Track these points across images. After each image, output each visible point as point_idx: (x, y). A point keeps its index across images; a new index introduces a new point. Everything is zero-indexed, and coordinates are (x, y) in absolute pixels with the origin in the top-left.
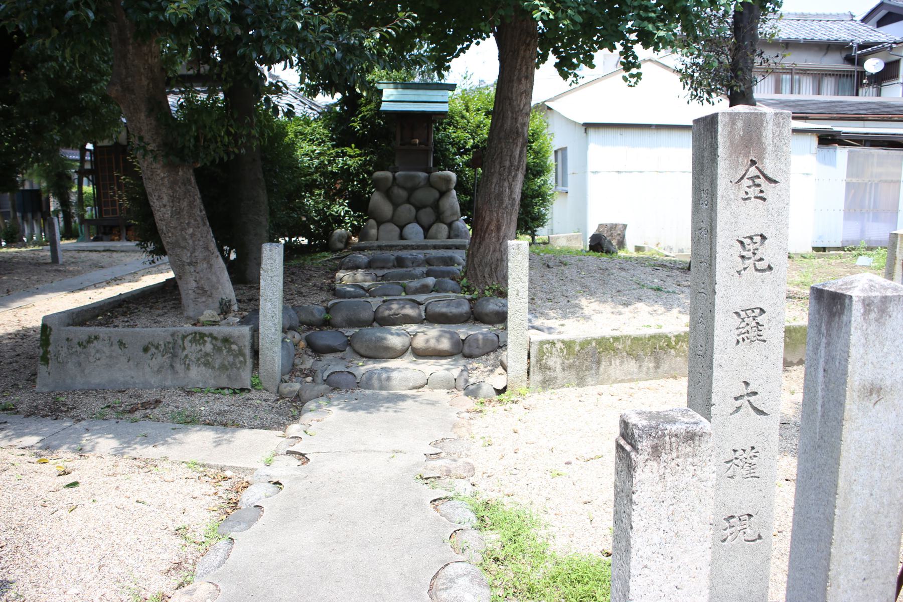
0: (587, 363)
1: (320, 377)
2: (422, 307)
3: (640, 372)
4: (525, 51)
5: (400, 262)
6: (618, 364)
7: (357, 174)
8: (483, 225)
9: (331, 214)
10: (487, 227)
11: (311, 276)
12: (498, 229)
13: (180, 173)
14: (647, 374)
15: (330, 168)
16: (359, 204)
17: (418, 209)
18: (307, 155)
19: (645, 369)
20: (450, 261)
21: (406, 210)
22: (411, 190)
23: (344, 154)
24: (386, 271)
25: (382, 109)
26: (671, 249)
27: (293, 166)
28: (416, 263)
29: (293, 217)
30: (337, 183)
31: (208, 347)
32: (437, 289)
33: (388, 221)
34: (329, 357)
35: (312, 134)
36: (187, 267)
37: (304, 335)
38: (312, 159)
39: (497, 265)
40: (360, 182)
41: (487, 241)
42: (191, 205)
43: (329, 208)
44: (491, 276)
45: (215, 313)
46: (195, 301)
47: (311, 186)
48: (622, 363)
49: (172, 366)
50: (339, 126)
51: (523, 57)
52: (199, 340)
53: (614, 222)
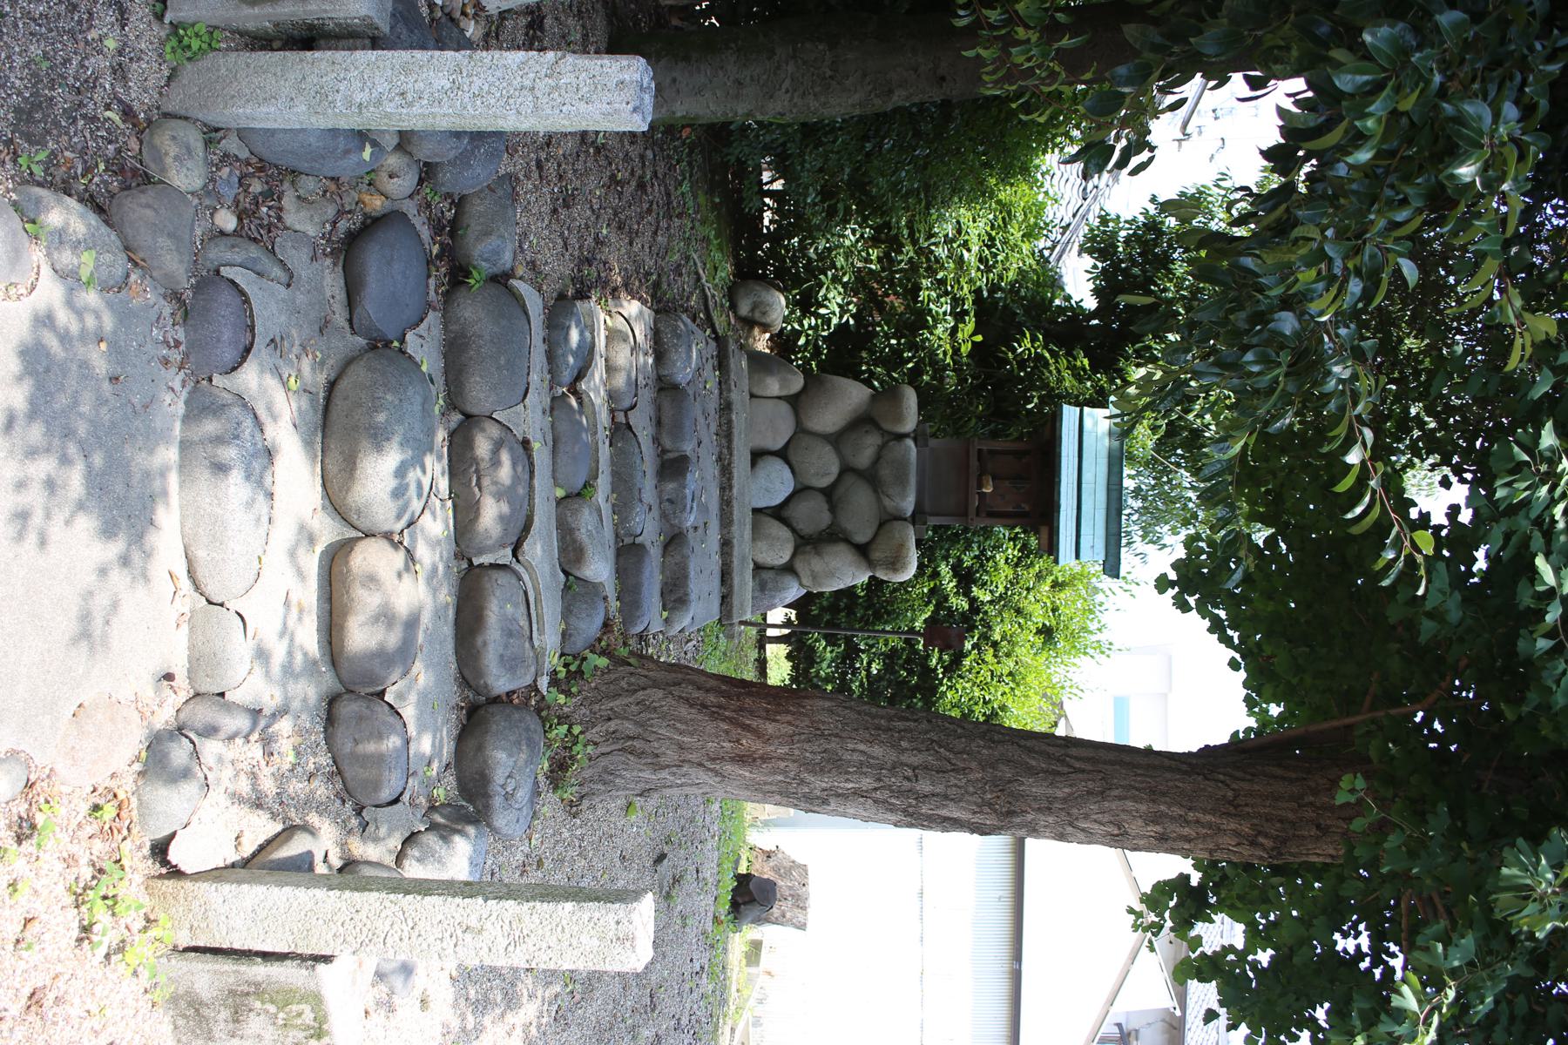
2: (505, 556)
4: (1236, 833)
5: (672, 467)
7: (913, 346)
8: (752, 713)
9: (821, 285)
10: (747, 728)
11: (632, 236)
12: (742, 759)
15: (926, 283)
16: (844, 352)
17: (828, 493)
18: (959, 232)
20: (675, 596)
21: (824, 466)
22: (871, 477)
23: (960, 317)
24: (644, 432)
25: (1066, 407)
26: (761, 1002)
27: (930, 197)
28: (671, 507)
29: (806, 196)
30: (891, 301)
32: (575, 589)
34: (332, 283)
35: (1005, 242)
37: (410, 208)
38: (948, 241)
39: (640, 755)
40: (896, 352)
41: (710, 727)
44: (612, 736)
47: (886, 238)
50: (1019, 307)
51: (1219, 830)
53: (813, 903)
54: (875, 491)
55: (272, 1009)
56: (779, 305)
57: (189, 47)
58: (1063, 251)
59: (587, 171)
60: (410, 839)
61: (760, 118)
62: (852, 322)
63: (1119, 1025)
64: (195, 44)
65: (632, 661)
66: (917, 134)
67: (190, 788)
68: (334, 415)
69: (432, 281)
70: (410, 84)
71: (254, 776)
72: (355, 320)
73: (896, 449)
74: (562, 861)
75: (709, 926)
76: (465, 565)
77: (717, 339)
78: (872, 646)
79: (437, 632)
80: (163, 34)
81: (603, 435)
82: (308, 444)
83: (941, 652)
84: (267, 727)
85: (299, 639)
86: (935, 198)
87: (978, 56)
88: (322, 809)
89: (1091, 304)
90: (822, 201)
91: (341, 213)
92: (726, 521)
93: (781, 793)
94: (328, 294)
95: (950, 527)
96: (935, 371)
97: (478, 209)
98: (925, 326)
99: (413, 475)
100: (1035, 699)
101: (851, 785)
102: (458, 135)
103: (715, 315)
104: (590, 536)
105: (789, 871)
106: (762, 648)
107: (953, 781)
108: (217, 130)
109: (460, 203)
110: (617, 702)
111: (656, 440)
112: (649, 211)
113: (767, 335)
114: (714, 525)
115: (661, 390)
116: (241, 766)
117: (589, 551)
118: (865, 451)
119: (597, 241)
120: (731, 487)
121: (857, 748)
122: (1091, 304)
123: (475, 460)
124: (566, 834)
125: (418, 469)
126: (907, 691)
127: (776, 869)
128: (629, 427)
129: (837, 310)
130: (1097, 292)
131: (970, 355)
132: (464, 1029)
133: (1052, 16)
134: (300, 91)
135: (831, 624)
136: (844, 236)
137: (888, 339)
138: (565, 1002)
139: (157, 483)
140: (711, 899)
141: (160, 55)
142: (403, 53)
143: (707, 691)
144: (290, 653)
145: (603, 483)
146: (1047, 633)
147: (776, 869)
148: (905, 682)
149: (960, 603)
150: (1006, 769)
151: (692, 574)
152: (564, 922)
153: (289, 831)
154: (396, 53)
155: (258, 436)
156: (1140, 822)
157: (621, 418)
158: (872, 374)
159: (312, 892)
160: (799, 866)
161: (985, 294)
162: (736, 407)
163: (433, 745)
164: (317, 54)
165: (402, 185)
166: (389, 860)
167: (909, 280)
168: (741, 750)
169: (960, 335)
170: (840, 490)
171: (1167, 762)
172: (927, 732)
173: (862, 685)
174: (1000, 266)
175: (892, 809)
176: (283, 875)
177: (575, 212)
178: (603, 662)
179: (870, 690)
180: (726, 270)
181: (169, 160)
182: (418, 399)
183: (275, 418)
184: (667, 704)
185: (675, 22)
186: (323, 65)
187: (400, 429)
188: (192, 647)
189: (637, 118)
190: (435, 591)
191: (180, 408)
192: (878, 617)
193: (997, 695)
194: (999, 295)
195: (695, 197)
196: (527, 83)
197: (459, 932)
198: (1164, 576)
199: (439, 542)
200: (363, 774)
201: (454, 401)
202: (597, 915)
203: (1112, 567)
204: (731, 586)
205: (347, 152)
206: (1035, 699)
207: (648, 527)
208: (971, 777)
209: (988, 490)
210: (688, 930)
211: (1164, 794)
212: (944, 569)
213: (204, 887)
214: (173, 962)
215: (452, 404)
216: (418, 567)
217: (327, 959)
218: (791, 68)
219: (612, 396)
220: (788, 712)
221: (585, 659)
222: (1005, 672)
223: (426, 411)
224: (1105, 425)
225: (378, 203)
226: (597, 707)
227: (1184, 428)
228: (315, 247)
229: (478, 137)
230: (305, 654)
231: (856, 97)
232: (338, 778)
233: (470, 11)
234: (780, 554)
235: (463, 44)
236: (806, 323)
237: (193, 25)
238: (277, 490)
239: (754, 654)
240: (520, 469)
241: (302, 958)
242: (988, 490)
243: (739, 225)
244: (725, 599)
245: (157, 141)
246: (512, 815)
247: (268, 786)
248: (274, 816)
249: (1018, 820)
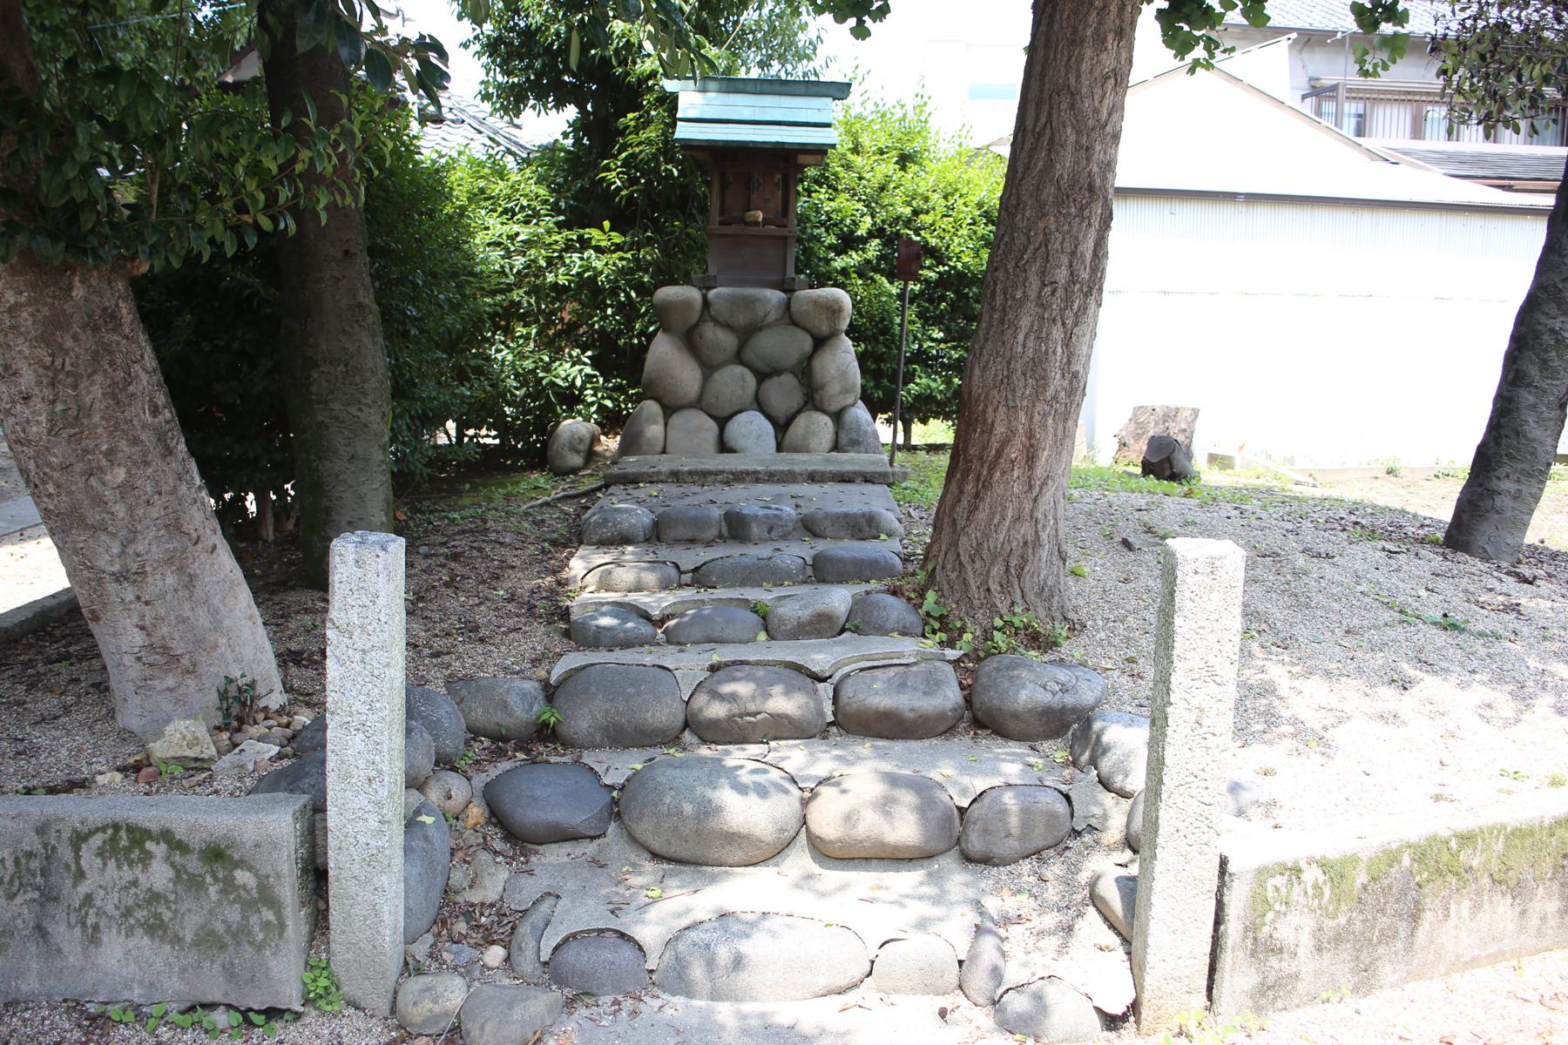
0: (1383, 921)
1: (530, 953)
2: (825, 690)
3: (1522, 929)
5: (736, 528)
6: (1465, 913)
7: (614, 292)
8: (984, 448)
9: (555, 384)
10: (999, 453)
12: (1031, 458)
13: (79, 292)
14: (1540, 933)
15: (550, 278)
16: (621, 361)
17: (762, 376)
18: (499, 244)
19: (1534, 919)
20: (864, 527)
21: (735, 381)
22: (746, 333)
23: (584, 244)
25: (677, 135)
27: (464, 274)
28: (776, 530)
29: (463, 396)
30: (576, 313)
31: (159, 875)
32: (857, 623)
33: (690, 406)
34: (554, 855)
35: (509, 198)
36: (112, 587)
37: (480, 780)
38: (508, 255)
40: (620, 308)
41: (998, 490)
42: (118, 394)
43: (547, 369)
44: (1005, 588)
45: (201, 730)
46: (143, 686)
47: (506, 317)
48: (1476, 908)
49: (41, 931)
50: (576, 185)
52: (128, 850)
53: (1173, 403)
54: (760, 329)
55: (1270, 916)
56: (573, 426)
57: (326, 988)
58: (516, 143)
59: (442, 609)
60: (1105, 784)
61: (387, 438)
62: (589, 353)
63: (1304, 97)
64: (323, 982)
65: (930, 567)
66: (401, 281)
67: (1052, 993)
68: (685, 854)
69: (553, 759)
70: (359, 775)
71: (1041, 934)
72: (592, 833)
73: (718, 308)
74: (1128, 639)
75: (1194, 501)
76: (834, 729)
77: (607, 486)
78: (916, 338)
79: (902, 756)
80: (314, 1013)
81: (705, 595)
82: (713, 879)
83: (922, 268)
84: (993, 920)
85: (909, 891)
86: (465, 268)
87: (326, 208)
88: (1074, 869)
89: (571, 112)
90: (469, 380)
91: (486, 847)
92: (789, 477)
93: (1066, 420)
94: (566, 859)
95: (797, 255)
96: (639, 269)
97: (481, 715)
98: (593, 279)
99: (745, 777)
100: (972, 173)
101: (1059, 350)
102: (409, 731)
103: (582, 489)
104: (805, 607)
105: (1139, 425)
106: (915, 448)
107: (1057, 246)
108: (406, 963)
109: (475, 732)
110: (972, 582)
111: (709, 544)
112: (480, 550)
113: (603, 438)
114: (794, 489)
115: (658, 539)
116: (1031, 946)
117: (820, 607)
118: (719, 339)
119: (511, 600)
120: (756, 472)
121: (1022, 343)
122: (571, 112)
123: (730, 718)
124: (1102, 635)
125: (739, 772)
126: (961, 302)
127: (1138, 437)
128: (696, 569)
129: (578, 367)
130: (559, 105)
131: (624, 234)
132: (1294, 736)
133: (285, 130)
134: (368, 881)
135: (893, 378)
136: (503, 361)
137: (607, 317)
138: (1268, 638)
139: (753, 1022)
140: (1168, 499)
141: (335, 1016)
142: (329, 780)
143: (962, 492)
144: (920, 898)
145: (752, 594)
146: (904, 160)
147: (1138, 437)
148: (952, 304)
149: (874, 248)
150: (1046, 191)
151: (844, 510)
152: (1195, 626)
153: (1095, 900)
154: (330, 786)
155: (705, 926)
156: (1103, 56)
157: (687, 578)
158: (642, 333)
159: (1157, 875)
160: (1135, 414)
161: (562, 218)
162: (675, 466)
163: (1012, 761)
164: (331, 864)
165: (458, 787)
166: (1126, 805)
167: (548, 295)
168: (1022, 460)
169: (603, 244)
170: (760, 365)
171: (1043, 28)
172: (1007, 272)
173: (954, 348)
174: (534, 203)
175: (1084, 309)
176: (1140, 904)
177: (481, 621)
178: (931, 596)
179: (959, 339)
180: (538, 478)
181: (437, 1008)
182: (670, 772)
183: (688, 911)
184: (974, 533)
185: (290, 526)
186: (342, 858)
187: (699, 790)
188: (914, 991)
189: (392, 547)
190: (859, 758)
191: (679, 1000)
193: (967, 212)
194: (562, 204)
195: (465, 507)
196: (358, 656)
197: (1201, 731)
198: (853, 31)
199: (811, 754)
200: (1040, 828)
201: (672, 739)
202: (1187, 594)
203: (839, 91)
205: (426, 839)
206: (972, 173)
207: (796, 552)
208: (1053, 227)
209: (760, 215)
210: (1198, 520)
211: (1075, 31)
212: (839, 263)
213: (1150, 980)
214: (1221, 1010)
215: (674, 740)
216: (836, 774)
217: (1223, 863)
218: (336, 406)
219: (665, 586)
220: (984, 411)
221: (928, 614)
222: (943, 202)
223: (682, 765)
224: (698, 98)
225: (475, 810)
226: (976, 602)
227: (699, 17)
228: (519, 872)
229: (411, 712)
230: (922, 884)
231: (366, 340)
232: (1044, 853)
233: (285, 720)
234: (822, 426)
235: (320, 725)
236: (590, 399)
237: (305, 984)
238: (760, 909)
239: (922, 455)
240: (739, 674)
241: (1222, 885)
242: (760, 215)
243: (491, 465)
244: (868, 479)
245: (418, 1020)
246: (1084, 685)
247: (1051, 920)
248: (1080, 915)
249: (1098, 181)
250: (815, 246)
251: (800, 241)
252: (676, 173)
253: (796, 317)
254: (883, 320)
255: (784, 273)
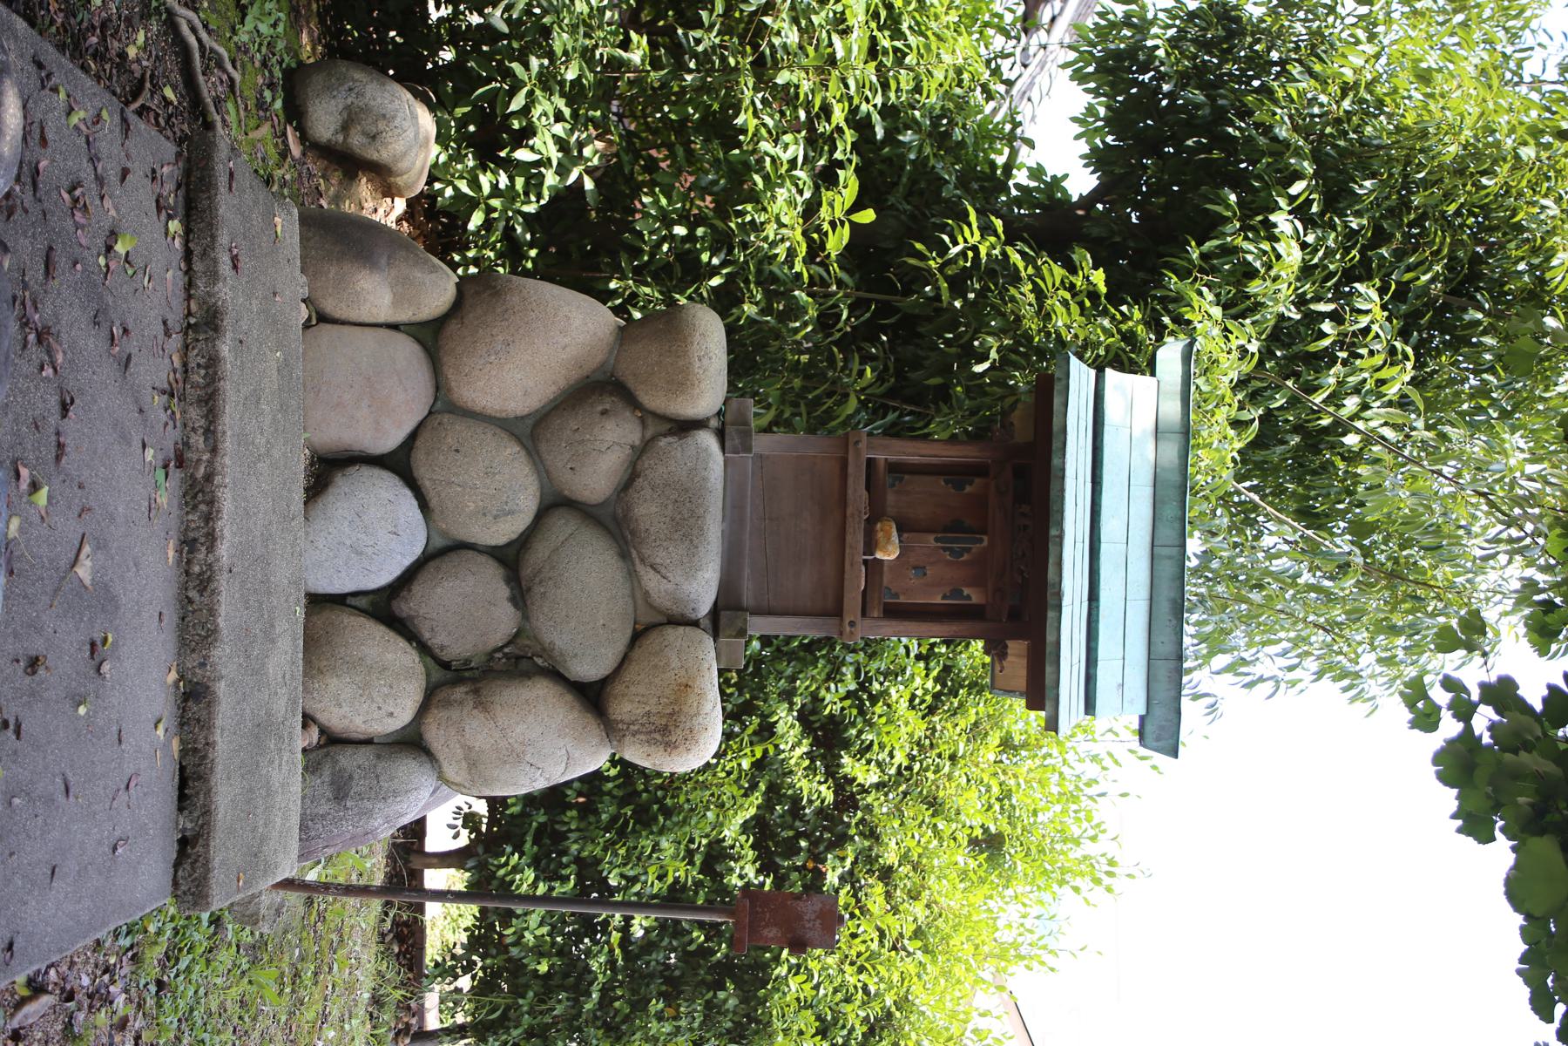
7: (722, 242)
9: (516, 86)
22: (614, 522)
43: (548, 81)
54: (624, 555)
56: (414, 135)
62: (589, 185)
73: (676, 456)
78: (633, 880)
89: (1081, 182)
92: (194, 626)
118: (600, 456)
120: (212, 539)
122: (1081, 182)
129: (555, 155)
130: (1098, 159)
131: (850, 253)
137: (668, 223)
146: (990, 845)
149: (815, 790)
169: (824, 212)
170: (540, 552)
173: (611, 962)
192: (645, 819)
196: (1006, 801)
203: (1161, 731)
204: (207, 812)
209: (888, 554)
212: (785, 720)
222: (909, 929)
236: (485, 180)
242: (888, 554)
250: (820, 669)
251: (829, 642)
252: (979, 368)
253: (652, 641)
254: (668, 812)
255: (758, 612)
